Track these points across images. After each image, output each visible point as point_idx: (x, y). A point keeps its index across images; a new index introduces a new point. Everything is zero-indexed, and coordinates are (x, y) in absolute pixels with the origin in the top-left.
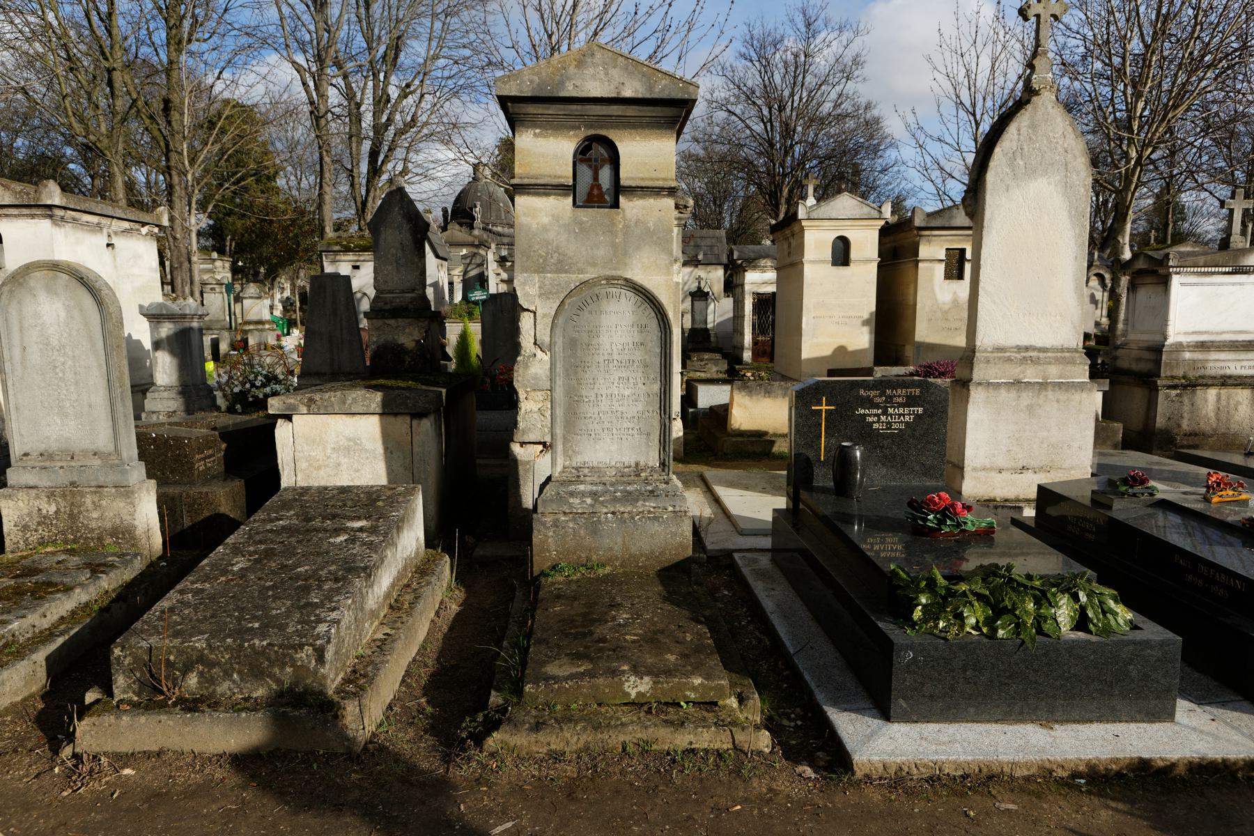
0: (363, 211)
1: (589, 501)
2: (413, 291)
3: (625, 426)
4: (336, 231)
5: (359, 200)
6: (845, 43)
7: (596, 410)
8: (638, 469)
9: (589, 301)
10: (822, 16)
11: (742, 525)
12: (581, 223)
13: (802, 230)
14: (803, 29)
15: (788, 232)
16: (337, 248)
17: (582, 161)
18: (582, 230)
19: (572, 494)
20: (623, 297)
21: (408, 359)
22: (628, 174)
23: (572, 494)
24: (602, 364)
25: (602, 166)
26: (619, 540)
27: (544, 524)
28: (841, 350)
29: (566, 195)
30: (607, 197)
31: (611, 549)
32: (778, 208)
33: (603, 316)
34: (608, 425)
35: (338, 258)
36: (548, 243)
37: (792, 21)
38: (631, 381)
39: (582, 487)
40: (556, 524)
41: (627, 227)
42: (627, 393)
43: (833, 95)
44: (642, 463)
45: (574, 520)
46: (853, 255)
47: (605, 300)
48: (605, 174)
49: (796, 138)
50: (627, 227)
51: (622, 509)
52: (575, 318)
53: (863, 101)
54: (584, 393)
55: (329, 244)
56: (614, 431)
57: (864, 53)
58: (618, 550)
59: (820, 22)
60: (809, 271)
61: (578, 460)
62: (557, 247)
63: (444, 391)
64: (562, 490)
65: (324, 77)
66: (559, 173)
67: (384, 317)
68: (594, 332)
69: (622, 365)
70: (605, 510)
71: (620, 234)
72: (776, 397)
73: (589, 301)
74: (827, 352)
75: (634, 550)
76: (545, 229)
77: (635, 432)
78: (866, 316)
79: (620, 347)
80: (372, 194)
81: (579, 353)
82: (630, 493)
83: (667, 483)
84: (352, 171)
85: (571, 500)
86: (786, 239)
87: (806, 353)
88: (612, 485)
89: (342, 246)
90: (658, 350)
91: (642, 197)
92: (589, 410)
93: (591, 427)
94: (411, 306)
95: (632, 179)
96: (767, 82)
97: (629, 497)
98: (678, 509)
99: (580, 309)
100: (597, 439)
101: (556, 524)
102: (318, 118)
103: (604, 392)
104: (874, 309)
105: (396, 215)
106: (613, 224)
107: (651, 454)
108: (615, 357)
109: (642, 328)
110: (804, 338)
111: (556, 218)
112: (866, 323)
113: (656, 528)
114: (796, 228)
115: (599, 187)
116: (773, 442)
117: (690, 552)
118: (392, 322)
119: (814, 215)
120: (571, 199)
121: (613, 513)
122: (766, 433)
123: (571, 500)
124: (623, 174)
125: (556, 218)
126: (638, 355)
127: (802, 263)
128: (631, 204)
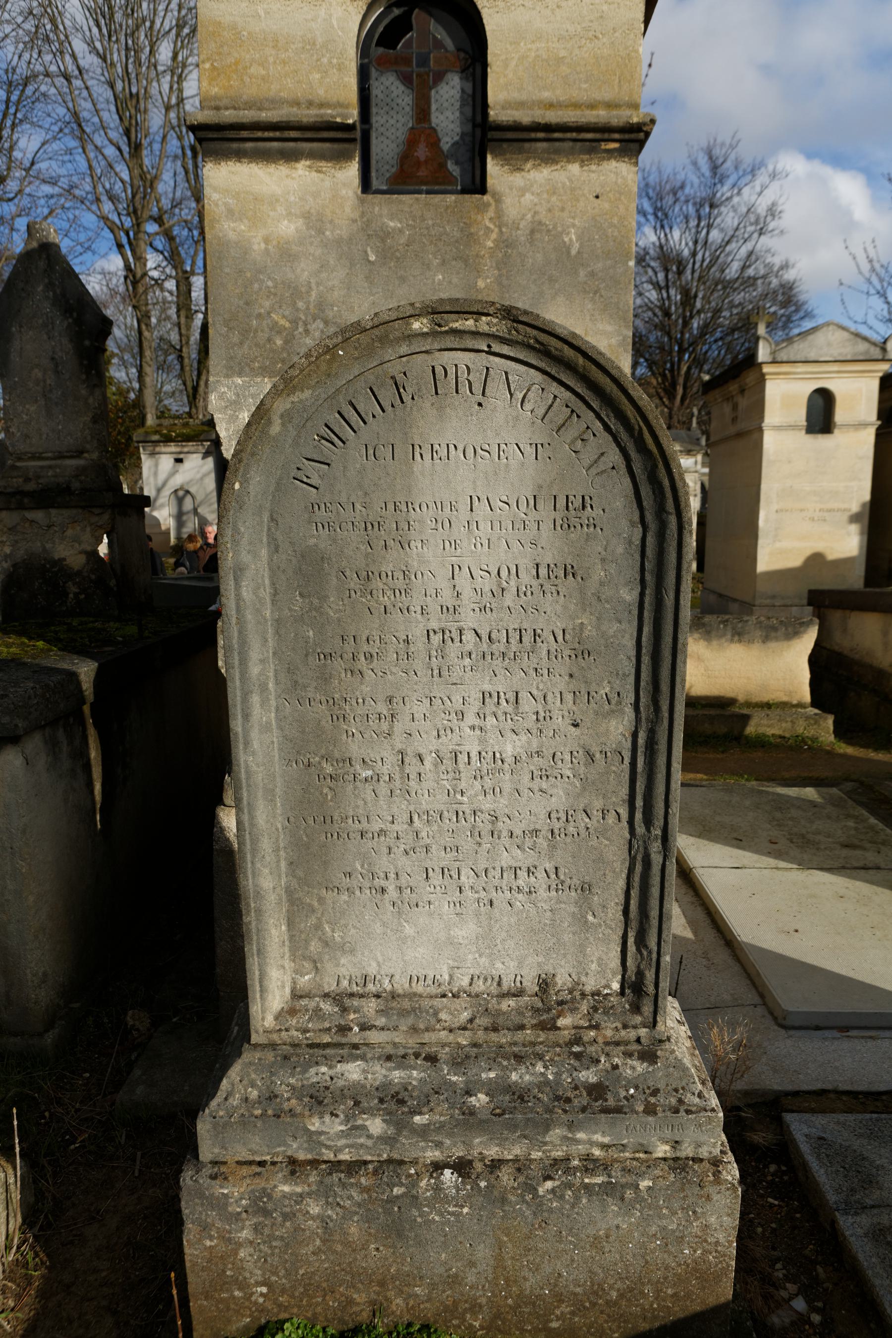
0: (195, 397)
1: (376, 1126)
2: (79, 453)
3: (505, 859)
4: (158, 418)
5: (189, 384)
6: (758, 189)
7: (401, 808)
8: (548, 1003)
9: (367, 405)
10: (732, 156)
11: (791, 999)
12: (384, 235)
13: (761, 380)
14: (708, 174)
15: (733, 387)
16: (156, 437)
17: (384, 64)
18: (385, 255)
19: (319, 1099)
20: (497, 387)
21: (73, 589)
22: (510, 90)
23: (319, 1099)
24: (419, 645)
25: (439, 77)
26: (483, 1253)
27: (221, 1204)
28: (816, 559)
29: (340, 157)
30: (452, 167)
31: (455, 1280)
32: (675, 388)
33: (422, 465)
34: (446, 860)
35: (158, 449)
36: (296, 292)
37: (695, 163)
38: (528, 705)
39: (353, 1071)
40: (261, 1205)
41: (506, 244)
42: (510, 747)
43: (743, 251)
44: (562, 980)
45: (324, 1192)
46: (839, 416)
47: (427, 403)
48: (449, 93)
49: (698, 305)
50: (506, 244)
51: (493, 1152)
52: (314, 472)
53: (777, 261)
54: (355, 749)
55: (147, 433)
56: (467, 878)
57: (781, 201)
58: (476, 1279)
59: (729, 164)
60: (770, 441)
61: (341, 972)
62: (321, 305)
63: (86, 671)
64: (285, 1083)
65: (141, 235)
66: (321, 93)
67: (21, 507)
68: (388, 528)
69: (491, 649)
70: (433, 1155)
71: (488, 265)
72: (751, 641)
73: (367, 405)
74: (795, 561)
75: (531, 1282)
76: (286, 253)
77: (540, 880)
78: (855, 508)
79: (487, 584)
80: (204, 378)
81: (334, 606)
82: (520, 1095)
83: (649, 1056)
84: (181, 350)
85: (314, 1124)
86: (729, 398)
87: (764, 564)
88: (459, 1062)
89: (162, 435)
90: (629, 595)
91: (548, 159)
92: (381, 809)
93: (383, 864)
94: (76, 485)
95: (521, 105)
96: (663, 241)
97: (517, 1109)
98: (687, 1150)
99: (332, 437)
100: (407, 902)
101: (261, 1205)
102: (135, 283)
103: (427, 745)
104: (867, 497)
105: (40, 300)
106: (470, 238)
107: (594, 952)
108: (469, 619)
109: (572, 511)
110: (761, 542)
111: (316, 222)
112: (855, 518)
113: (612, 1217)
114: (750, 378)
115: (434, 140)
116: (746, 718)
117: (725, 1291)
118: (38, 515)
119: (782, 356)
120: (352, 170)
121: (462, 1167)
122: (732, 702)
123: (314, 1124)
124: (495, 94)
125: (316, 222)
126: (553, 614)
127: (760, 430)
128: (518, 179)
